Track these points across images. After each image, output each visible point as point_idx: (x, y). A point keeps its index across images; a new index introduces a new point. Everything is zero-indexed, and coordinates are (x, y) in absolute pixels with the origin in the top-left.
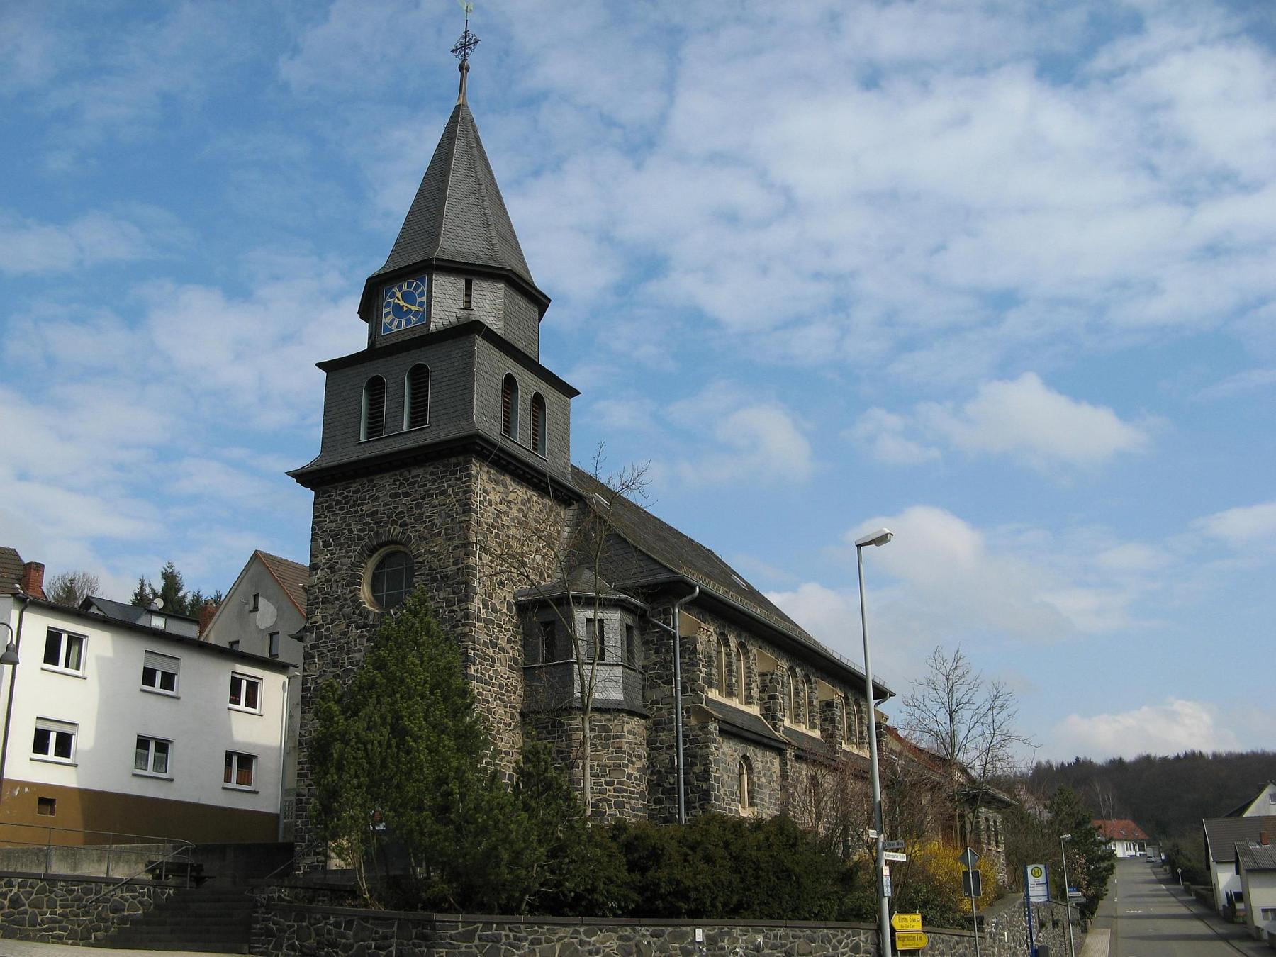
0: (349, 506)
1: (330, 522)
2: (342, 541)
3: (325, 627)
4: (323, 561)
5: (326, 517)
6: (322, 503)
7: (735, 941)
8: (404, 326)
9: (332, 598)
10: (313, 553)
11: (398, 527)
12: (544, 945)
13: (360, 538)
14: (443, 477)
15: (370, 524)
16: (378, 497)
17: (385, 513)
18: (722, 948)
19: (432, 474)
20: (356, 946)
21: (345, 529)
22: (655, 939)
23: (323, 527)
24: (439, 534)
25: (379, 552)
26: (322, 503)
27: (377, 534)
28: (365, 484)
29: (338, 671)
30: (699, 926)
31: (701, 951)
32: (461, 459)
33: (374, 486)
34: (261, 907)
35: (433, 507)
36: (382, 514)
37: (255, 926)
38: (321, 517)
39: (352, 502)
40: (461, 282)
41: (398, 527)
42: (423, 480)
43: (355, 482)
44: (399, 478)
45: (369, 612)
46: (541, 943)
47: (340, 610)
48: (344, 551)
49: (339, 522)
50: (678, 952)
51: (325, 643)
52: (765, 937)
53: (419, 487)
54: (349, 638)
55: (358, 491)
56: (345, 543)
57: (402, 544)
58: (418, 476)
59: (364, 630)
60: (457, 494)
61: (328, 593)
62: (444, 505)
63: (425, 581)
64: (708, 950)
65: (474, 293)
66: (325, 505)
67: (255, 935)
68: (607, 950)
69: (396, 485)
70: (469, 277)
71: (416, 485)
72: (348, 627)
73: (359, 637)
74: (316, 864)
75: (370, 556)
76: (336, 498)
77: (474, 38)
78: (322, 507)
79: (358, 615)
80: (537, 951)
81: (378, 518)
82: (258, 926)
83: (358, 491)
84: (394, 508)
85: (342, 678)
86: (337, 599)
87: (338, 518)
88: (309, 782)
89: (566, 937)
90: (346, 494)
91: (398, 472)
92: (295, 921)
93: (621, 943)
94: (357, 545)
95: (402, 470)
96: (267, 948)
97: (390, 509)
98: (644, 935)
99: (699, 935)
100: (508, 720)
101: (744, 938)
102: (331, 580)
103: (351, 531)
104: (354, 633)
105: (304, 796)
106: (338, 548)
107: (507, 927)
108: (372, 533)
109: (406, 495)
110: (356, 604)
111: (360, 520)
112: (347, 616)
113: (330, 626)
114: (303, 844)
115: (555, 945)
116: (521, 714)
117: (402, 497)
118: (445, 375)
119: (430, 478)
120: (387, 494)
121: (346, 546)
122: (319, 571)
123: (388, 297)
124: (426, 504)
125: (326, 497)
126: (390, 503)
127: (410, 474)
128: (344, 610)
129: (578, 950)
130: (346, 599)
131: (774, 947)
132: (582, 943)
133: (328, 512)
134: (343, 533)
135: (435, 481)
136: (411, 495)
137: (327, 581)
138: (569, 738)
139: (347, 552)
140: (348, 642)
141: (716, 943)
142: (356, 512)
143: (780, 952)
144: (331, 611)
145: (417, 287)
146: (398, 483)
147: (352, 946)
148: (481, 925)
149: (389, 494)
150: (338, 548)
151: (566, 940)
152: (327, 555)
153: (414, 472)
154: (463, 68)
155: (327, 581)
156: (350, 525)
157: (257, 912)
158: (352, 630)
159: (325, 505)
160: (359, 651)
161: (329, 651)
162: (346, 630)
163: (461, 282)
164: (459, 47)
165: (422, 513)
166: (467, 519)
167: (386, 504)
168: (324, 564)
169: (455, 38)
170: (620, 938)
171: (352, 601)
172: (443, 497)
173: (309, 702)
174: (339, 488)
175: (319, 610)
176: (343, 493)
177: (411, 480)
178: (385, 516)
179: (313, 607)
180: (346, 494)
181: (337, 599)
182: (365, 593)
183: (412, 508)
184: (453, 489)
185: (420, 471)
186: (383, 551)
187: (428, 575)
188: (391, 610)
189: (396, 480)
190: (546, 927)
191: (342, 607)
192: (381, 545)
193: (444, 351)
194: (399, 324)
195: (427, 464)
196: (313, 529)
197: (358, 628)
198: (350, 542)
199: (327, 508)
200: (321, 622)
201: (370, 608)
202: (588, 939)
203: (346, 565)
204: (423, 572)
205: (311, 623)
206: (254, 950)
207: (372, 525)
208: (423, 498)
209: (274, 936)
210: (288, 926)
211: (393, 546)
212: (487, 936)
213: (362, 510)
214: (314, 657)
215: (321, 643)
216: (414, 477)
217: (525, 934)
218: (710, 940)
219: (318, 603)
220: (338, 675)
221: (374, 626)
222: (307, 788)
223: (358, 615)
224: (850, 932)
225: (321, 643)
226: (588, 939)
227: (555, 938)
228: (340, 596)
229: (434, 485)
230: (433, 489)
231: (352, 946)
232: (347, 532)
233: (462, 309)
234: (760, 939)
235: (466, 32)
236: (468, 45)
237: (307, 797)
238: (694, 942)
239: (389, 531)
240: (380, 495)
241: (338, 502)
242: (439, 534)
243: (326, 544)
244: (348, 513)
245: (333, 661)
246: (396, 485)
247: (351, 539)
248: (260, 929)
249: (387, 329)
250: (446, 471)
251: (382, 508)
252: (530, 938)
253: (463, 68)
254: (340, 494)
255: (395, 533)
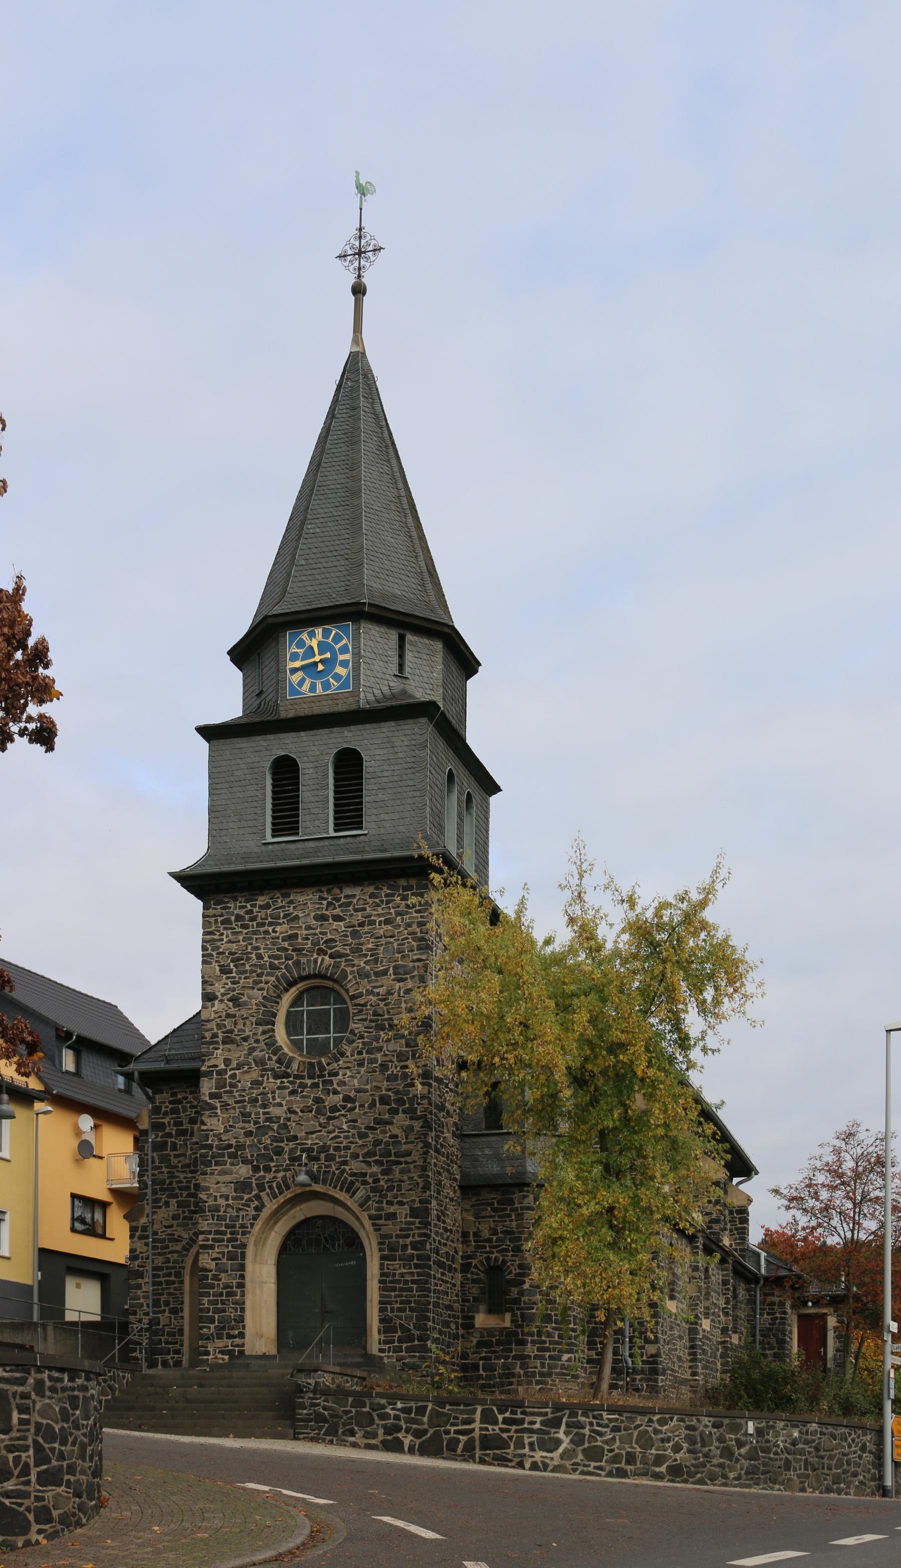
0: (255, 923)
1: (230, 942)
2: (248, 968)
3: (229, 1073)
4: (222, 991)
5: (222, 934)
6: (214, 916)
7: (777, 1435)
8: (319, 689)
9: (238, 1038)
10: (207, 979)
11: (327, 958)
12: (623, 1432)
13: (273, 967)
14: (388, 902)
15: (287, 950)
16: (297, 918)
17: (308, 939)
18: (768, 1441)
19: (372, 896)
20: (431, 1431)
21: (251, 953)
22: (715, 1430)
23: (218, 948)
24: (385, 973)
25: (298, 986)
26: (214, 916)
27: (297, 963)
28: (278, 898)
29: (252, 1127)
30: (750, 1419)
31: (752, 1442)
32: (413, 882)
33: (291, 902)
34: (307, 1392)
35: (376, 938)
36: (304, 939)
37: (300, 1411)
38: (215, 935)
39: (259, 920)
40: (393, 635)
41: (327, 958)
42: (361, 902)
43: (262, 895)
44: (326, 896)
45: (291, 1059)
46: (620, 1431)
47: (250, 1054)
48: (251, 981)
49: (241, 943)
50: (734, 1443)
51: (231, 1092)
52: (800, 1432)
53: (357, 910)
54: (264, 1088)
55: (267, 906)
56: (252, 972)
57: (335, 981)
58: (354, 896)
59: (285, 1080)
60: (409, 925)
61: (231, 1031)
62: (391, 937)
63: (368, 1028)
64: (757, 1442)
65: (409, 656)
66: (220, 919)
67: (302, 1420)
68: (676, 1439)
69: (322, 904)
70: (402, 632)
71: (351, 908)
72: (262, 1076)
73: (279, 1088)
74: (230, 1348)
75: (287, 990)
76: (236, 912)
77: (373, 242)
78: (216, 921)
79: (276, 1062)
80: (617, 1438)
81: (298, 944)
82: (305, 1411)
83: (267, 906)
84: (321, 933)
85: (256, 1136)
86: (245, 1039)
87: (241, 938)
88: (215, 1255)
89: (641, 1425)
90: (249, 908)
91: (324, 889)
92: (351, 1407)
93: (688, 1432)
94: (271, 975)
95: (331, 886)
96: (319, 1434)
97: (315, 934)
98: (706, 1426)
99: (751, 1427)
100: (451, 1194)
101: (785, 1432)
102: (234, 1016)
103: (260, 957)
104: (271, 1083)
105: (211, 1271)
106: (243, 977)
107: (590, 1415)
108: (290, 962)
109: (337, 918)
110: (271, 1043)
111: (273, 944)
112: (260, 1062)
113: (237, 1072)
114: (212, 1326)
115: (632, 1433)
116: (461, 1187)
117: (331, 921)
118: (385, 767)
119: (370, 901)
120: (309, 914)
121: (254, 974)
122: (216, 1002)
123: (293, 645)
124: (366, 933)
125: (221, 908)
126: (314, 926)
127: (341, 892)
128: (255, 1054)
129: (652, 1438)
130: (257, 1041)
131: (807, 1442)
132: (656, 1431)
133: (225, 929)
134: (249, 959)
135: (378, 906)
136: (345, 920)
137: (228, 1016)
138: (520, 1217)
139: (256, 983)
140: (262, 1094)
141: (763, 1436)
142: (267, 932)
143: (810, 1447)
144: (237, 1054)
145: (337, 639)
146: (325, 902)
147: (425, 1432)
148: (567, 1412)
149: (312, 914)
150: (243, 977)
151: (641, 1428)
152: (227, 984)
153: (348, 891)
154: (359, 290)
155: (228, 1016)
156: (258, 948)
157: (303, 1398)
158: (268, 1079)
159: (220, 919)
160: (280, 1105)
161: (236, 1102)
162: (260, 1079)
163: (393, 635)
164: (350, 252)
165: (362, 944)
166: (424, 957)
167: (309, 928)
168: (223, 995)
169: (345, 238)
170: (688, 1428)
171: (266, 1044)
172: (389, 927)
173: (210, 1162)
174: (240, 899)
175: (219, 1051)
176: (245, 907)
177: (343, 900)
178: (309, 942)
179: (211, 1047)
180: (249, 908)
181: (245, 1039)
182: (281, 1035)
183: (346, 936)
184: (403, 919)
185: (357, 891)
186: (301, 986)
187: (371, 1021)
188: (323, 1060)
189: (321, 898)
190: (625, 1415)
191: (252, 1050)
192: (302, 979)
193: (382, 735)
194: (313, 688)
195: (366, 883)
196: (204, 948)
197: (276, 1077)
198: (259, 971)
199: (223, 923)
200: (222, 1066)
201: (291, 1054)
202: (660, 1428)
203: (256, 999)
204: (364, 1017)
205: (209, 1067)
206: (301, 1436)
207: (290, 952)
208: (361, 925)
209: (325, 1421)
210: (343, 1411)
211: (318, 981)
212: (573, 1422)
213: (274, 931)
214: (216, 1108)
215: (225, 1092)
216: (346, 897)
217: (606, 1422)
218: (759, 1432)
219: (217, 1043)
220: (251, 1132)
221: (297, 1077)
222: (214, 1263)
223: (276, 1062)
224: (860, 1432)
225: (225, 1092)
226: (660, 1428)
227: (632, 1426)
228: (248, 1036)
229: (376, 910)
230: (375, 915)
231: (425, 1432)
232: (254, 958)
233: (395, 675)
234: (796, 1434)
235: (360, 230)
236: (365, 252)
237: (214, 1272)
238: (746, 1434)
239: (316, 961)
240: (301, 915)
241: (239, 918)
242: (385, 973)
243: (225, 970)
244: (255, 933)
245: (244, 1115)
246: (322, 904)
247: (261, 967)
248: (306, 1414)
249: (294, 691)
250: (393, 895)
251: (305, 932)
252: (611, 1425)
253: (359, 290)
254: (241, 907)
255: (324, 965)
